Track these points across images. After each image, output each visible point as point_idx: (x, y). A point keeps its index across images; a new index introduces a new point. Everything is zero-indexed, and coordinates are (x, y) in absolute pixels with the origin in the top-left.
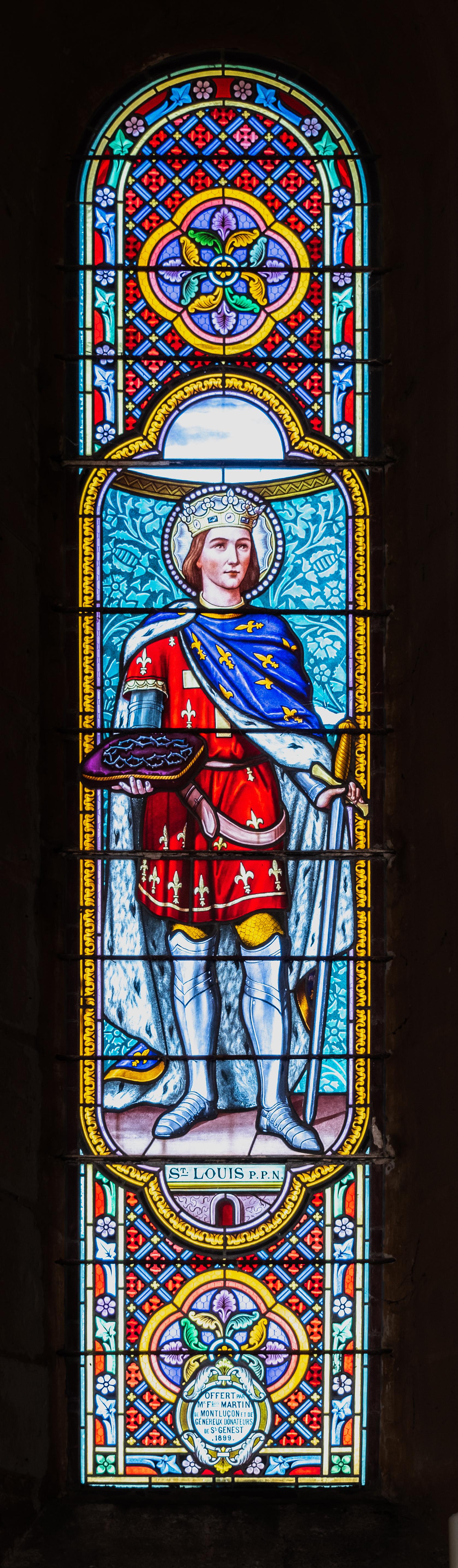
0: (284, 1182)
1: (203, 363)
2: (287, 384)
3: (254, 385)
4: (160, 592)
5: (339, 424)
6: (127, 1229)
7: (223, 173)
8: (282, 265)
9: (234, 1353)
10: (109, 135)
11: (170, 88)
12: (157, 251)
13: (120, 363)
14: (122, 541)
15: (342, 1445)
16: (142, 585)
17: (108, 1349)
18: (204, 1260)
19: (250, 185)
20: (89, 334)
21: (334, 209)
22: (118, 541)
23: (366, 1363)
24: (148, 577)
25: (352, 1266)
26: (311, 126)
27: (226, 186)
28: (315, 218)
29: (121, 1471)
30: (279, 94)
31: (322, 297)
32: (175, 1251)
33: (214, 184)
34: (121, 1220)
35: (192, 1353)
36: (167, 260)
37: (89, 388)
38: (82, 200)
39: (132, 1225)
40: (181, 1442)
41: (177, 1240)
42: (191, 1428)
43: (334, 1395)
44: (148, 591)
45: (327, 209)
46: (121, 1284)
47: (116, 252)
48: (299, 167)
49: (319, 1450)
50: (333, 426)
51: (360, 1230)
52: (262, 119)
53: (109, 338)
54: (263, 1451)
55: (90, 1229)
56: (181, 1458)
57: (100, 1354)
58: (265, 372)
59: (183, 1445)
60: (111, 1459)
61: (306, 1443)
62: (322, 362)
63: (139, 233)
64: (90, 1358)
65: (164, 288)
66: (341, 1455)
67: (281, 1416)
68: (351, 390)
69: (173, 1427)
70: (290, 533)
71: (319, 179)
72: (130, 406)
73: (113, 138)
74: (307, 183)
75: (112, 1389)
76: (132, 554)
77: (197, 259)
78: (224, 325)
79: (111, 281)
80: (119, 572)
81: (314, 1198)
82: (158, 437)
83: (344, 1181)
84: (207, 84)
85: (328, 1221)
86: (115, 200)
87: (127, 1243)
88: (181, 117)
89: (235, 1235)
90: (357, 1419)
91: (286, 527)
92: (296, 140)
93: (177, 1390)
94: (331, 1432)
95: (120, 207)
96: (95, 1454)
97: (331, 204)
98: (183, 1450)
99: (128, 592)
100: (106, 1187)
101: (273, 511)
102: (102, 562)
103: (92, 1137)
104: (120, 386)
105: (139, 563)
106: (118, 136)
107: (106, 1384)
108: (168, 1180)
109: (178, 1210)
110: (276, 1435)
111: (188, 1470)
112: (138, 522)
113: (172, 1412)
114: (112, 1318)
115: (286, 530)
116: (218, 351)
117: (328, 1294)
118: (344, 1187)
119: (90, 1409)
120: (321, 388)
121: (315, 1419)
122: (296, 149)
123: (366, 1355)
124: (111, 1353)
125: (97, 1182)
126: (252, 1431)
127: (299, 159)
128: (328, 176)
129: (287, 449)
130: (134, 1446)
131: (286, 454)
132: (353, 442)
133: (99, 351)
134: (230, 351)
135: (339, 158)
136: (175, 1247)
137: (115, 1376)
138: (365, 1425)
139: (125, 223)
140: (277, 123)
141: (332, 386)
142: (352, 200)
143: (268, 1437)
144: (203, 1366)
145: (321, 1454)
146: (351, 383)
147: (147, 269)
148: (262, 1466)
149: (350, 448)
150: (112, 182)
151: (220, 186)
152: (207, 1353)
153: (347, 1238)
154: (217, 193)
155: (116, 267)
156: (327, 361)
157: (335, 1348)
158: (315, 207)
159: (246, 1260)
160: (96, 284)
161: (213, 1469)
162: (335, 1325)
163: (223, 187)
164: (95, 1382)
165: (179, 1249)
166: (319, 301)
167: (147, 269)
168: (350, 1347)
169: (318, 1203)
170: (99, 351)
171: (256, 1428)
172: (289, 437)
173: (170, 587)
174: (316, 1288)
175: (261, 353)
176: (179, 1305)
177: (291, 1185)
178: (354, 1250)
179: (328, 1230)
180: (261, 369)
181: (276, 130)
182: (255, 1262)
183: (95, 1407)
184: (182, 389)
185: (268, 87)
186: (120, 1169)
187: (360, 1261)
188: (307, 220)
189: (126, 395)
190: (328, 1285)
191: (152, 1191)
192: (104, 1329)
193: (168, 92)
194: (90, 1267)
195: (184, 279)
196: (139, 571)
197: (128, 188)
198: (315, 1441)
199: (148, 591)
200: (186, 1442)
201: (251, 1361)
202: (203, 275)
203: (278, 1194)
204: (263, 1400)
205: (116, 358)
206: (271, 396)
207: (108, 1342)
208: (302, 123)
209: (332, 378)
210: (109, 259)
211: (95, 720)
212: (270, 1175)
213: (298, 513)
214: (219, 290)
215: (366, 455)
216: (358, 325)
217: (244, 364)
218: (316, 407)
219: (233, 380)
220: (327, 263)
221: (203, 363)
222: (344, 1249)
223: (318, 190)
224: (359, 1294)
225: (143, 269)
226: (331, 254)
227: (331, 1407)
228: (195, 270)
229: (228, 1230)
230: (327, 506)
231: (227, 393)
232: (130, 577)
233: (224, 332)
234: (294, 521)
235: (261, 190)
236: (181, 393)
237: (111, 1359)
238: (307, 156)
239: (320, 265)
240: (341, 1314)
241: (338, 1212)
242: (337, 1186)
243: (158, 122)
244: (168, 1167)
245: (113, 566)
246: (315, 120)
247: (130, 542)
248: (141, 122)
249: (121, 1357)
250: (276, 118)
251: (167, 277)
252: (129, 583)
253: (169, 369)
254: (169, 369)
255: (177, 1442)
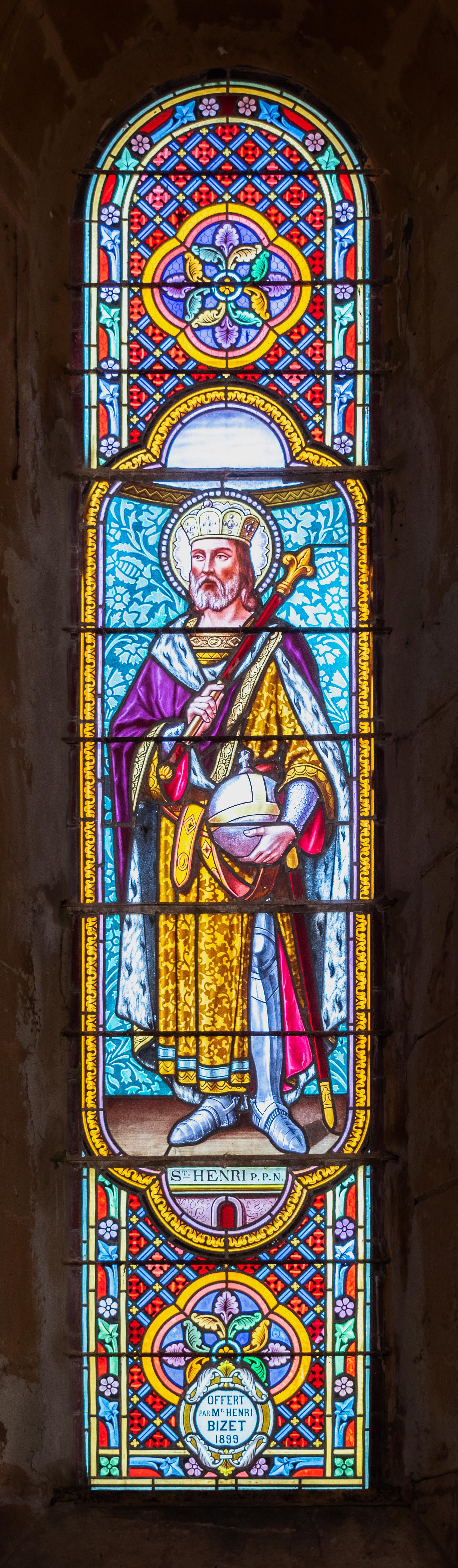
0: (285, 1185)
1: (206, 377)
2: (289, 396)
3: (256, 398)
4: (162, 603)
5: (340, 435)
6: (129, 1231)
7: (227, 189)
8: (284, 279)
9: (235, 1355)
10: (115, 153)
11: (174, 106)
12: (162, 267)
13: (125, 377)
14: (124, 554)
15: (344, 1447)
16: (144, 597)
17: (110, 1350)
18: (205, 1262)
19: (253, 200)
20: (94, 350)
21: (337, 224)
22: (121, 554)
23: (368, 1364)
24: (150, 588)
25: (353, 1267)
26: (314, 141)
27: (230, 201)
28: (318, 232)
29: (124, 1474)
30: (282, 109)
31: (323, 311)
32: (176, 1253)
33: (218, 199)
34: (123, 1223)
35: (194, 1355)
36: (171, 276)
37: (94, 403)
38: (87, 218)
39: (135, 1229)
40: (184, 1444)
41: (179, 1243)
42: (194, 1431)
43: (336, 1397)
44: (151, 603)
45: (329, 223)
46: (123, 1287)
47: (119, 270)
48: (303, 181)
49: (321, 1452)
50: (333, 437)
51: (361, 1232)
52: (267, 136)
53: (114, 354)
54: (266, 1452)
55: (92, 1231)
56: (184, 1460)
57: (103, 1357)
58: (268, 385)
59: (186, 1447)
60: (115, 1461)
61: (309, 1445)
62: (324, 373)
63: (143, 250)
64: (93, 1360)
65: (169, 306)
66: (344, 1457)
67: (283, 1417)
68: (352, 402)
69: (176, 1429)
70: (290, 541)
71: (322, 193)
72: (135, 420)
73: (119, 157)
74: (309, 196)
75: (115, 1391)
76: (134, 566)
77: (200, 275)
78: (227, 339)
79: (116, 298)
80: (122, 584)
81: (315, 1200)
82: (162, 450)
83: (345, 1183)
84: (213, 101)
85: (330, 1222)
86: (120, 217)
87: (129, 1246)
88: (185, 135)
89: (237, 1237)
90: (360, 1421)
91: (285, 535)
92: (299, 155)
93: (180, 1392)
94: (332, 1431)
95: (125, 225)
96: (99, 1456)
97: (333, 217)
98: (187, 1453)
99: (131, 603)
100: (108, 1189)
101: (273, 518)
102: (105, 574)
103: (94, 1140)
104: (125, 400)
105: (141, 575)
106: (124, 156)
107: (110, 1386)
108: (170, 1182)
109: (180, 1213)
110: (280, 1436)
111: (190, 1473)
112: (141, 535)
113: (176, 1414)
114: (114, 1319)
115: (285, 539)
116: (221, 364)
117: (329, 1295)
118: (345, 1191)
119: (93, 1411)
120: (322, 399)
121: (317, 1422)
122: (299, 164)
123: (368, 1357)
124: (114, 1355)
125: (100, 1185)
126: (255, 1433)
127: (301, 174)
128: (330, 190)
129: (289, 460)
130: (138, 1448)
131: (287, 465)
132: (353, 453)
133: (104, 365)
134: (233, 364)
135: (341, 172)
136: (177, 1249)
137: (117, 1378)
138: (367, 1426)
139: (130, 240)
140: (280, 139)
141: (334, 398)
142: (355, 213)
143: (271, 1439)
144: (205, 1367)
145: (324, 1456)
146: (351, 395)
147: (152, 286)
148: (266, 1467)
149: (351, 459)
150: (117, 200)
151: (224, 201)
152: (209, 1355)
153: (348, 1239)
154: (221, 208)
155: (121, 285)
156: (329, 372)
157: (337, 1350)
158: (317, 220)
159: (248, 1262)
160: (100, 300)
161: (215, 1471)
162: (338, 1326)
163: (227, 203)
164: (98, 1384)
165: (181, 1252)
166: (321, 315)
167: (152, 286)
168: (352, 1349)
169: (318, 1205)
170: (104, 365)
171: (259, 1430)
172: (290, 448)
173: (172, 598)
174: (318, 1288)
175: (263, 366)
176: (182, 1307)
177: (292, 1187)
178: (355, 1251)
179: (330, 1232)
180: (264, 381)
181: (280, 146)
182: (256, 1263)
183: (98, 1408)
184: (185, 402)
185: (270, 102)
186: (121, 1173)
187: (361, 1261)
188: (310, 233)
189: (130, 408)
190: (329, 1285)
191: (154, 1196)
192: (107, 1331)
193: (173, 110)
194: (92, 1268)
195: (188, 294)
196: (142, 583)
197: (134, 207)
198: (318, 1443)
199: (151, 603)
200: (189, 1444)
201: (253, 1362)
202: (207, 291)
203: (279, 1196)
204: (266, 1402)
205: (120, 372)
206: (274, 408)
207: (110, 1344)
208: (306, 138)
209: (334, 391)
210: (115, 277)
211: (95, 727)
212: (271, 1176)
213: (298, 521)
214: (222, 305)
215: (367, 464)
216: (360, 339)
217: (247, 377)
218: (317, 418)
219: (237, 393)
220: (329, 276)
221: (206, 377)
222: (345, 1250)
223: (321, 204)
224: (361, 1295)
225: (147, 285)
226: (334, 268)
227: (334, 1408)
228: (197, 285)
229: (230, 1233)
230: (326, 513)
231: (230, 405)
232: (132, 589)
233: (226, 346)
234: (295, 529)
235: (265, 204)
236: (184, 406)
237: (113, 1361)
238: (310, 171)
239: (322, 278)
240: (342, 1315)
241: (339, 1213)
242: (338, 1188)
243: (163, 140)
244: (170, 1170)
245: (116, 578)
246: (318, 135)
247: (132, 555)
248: (146, 140)
249: (124, 1360)
250: (279, 133)
251: (170, 294)
252: (132, 594)
253: (173, 382)
254: (173, 382)
255: (180, 1444)
